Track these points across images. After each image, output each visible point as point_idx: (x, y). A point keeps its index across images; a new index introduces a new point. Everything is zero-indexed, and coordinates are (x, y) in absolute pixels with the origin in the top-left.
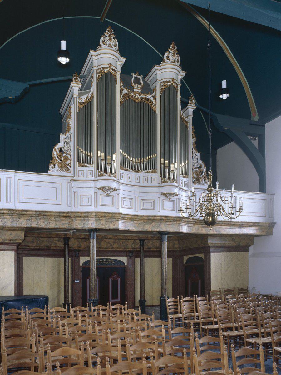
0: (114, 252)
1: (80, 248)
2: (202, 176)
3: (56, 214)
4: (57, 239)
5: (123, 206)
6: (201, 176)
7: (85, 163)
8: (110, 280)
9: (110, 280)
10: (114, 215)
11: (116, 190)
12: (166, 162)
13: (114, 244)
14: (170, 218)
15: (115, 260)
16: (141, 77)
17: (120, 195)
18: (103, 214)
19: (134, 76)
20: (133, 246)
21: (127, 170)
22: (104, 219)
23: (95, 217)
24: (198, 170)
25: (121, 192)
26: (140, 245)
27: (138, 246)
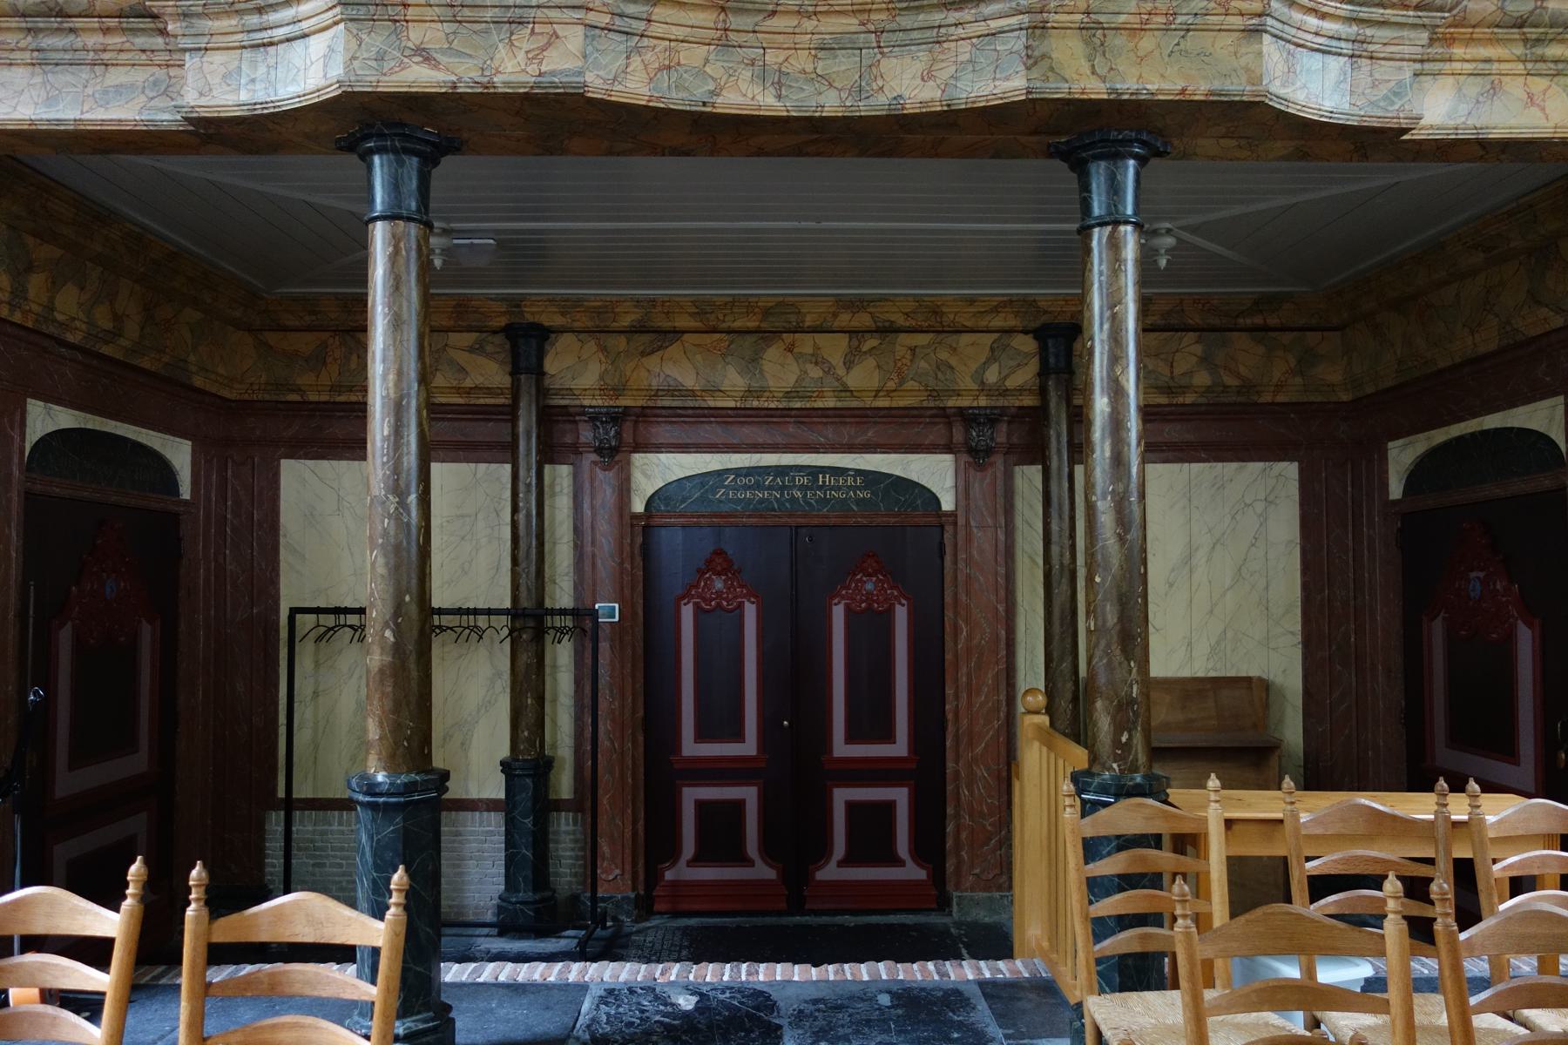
0: (863, 416)
1: (618, 391)
4: (469, 338)
8: (838, 613)
9: (838, 613)
13: (849, 365)
15: (872, 478)
20: (992, 376)
26: (1044, 373)
27: (1025, 375)
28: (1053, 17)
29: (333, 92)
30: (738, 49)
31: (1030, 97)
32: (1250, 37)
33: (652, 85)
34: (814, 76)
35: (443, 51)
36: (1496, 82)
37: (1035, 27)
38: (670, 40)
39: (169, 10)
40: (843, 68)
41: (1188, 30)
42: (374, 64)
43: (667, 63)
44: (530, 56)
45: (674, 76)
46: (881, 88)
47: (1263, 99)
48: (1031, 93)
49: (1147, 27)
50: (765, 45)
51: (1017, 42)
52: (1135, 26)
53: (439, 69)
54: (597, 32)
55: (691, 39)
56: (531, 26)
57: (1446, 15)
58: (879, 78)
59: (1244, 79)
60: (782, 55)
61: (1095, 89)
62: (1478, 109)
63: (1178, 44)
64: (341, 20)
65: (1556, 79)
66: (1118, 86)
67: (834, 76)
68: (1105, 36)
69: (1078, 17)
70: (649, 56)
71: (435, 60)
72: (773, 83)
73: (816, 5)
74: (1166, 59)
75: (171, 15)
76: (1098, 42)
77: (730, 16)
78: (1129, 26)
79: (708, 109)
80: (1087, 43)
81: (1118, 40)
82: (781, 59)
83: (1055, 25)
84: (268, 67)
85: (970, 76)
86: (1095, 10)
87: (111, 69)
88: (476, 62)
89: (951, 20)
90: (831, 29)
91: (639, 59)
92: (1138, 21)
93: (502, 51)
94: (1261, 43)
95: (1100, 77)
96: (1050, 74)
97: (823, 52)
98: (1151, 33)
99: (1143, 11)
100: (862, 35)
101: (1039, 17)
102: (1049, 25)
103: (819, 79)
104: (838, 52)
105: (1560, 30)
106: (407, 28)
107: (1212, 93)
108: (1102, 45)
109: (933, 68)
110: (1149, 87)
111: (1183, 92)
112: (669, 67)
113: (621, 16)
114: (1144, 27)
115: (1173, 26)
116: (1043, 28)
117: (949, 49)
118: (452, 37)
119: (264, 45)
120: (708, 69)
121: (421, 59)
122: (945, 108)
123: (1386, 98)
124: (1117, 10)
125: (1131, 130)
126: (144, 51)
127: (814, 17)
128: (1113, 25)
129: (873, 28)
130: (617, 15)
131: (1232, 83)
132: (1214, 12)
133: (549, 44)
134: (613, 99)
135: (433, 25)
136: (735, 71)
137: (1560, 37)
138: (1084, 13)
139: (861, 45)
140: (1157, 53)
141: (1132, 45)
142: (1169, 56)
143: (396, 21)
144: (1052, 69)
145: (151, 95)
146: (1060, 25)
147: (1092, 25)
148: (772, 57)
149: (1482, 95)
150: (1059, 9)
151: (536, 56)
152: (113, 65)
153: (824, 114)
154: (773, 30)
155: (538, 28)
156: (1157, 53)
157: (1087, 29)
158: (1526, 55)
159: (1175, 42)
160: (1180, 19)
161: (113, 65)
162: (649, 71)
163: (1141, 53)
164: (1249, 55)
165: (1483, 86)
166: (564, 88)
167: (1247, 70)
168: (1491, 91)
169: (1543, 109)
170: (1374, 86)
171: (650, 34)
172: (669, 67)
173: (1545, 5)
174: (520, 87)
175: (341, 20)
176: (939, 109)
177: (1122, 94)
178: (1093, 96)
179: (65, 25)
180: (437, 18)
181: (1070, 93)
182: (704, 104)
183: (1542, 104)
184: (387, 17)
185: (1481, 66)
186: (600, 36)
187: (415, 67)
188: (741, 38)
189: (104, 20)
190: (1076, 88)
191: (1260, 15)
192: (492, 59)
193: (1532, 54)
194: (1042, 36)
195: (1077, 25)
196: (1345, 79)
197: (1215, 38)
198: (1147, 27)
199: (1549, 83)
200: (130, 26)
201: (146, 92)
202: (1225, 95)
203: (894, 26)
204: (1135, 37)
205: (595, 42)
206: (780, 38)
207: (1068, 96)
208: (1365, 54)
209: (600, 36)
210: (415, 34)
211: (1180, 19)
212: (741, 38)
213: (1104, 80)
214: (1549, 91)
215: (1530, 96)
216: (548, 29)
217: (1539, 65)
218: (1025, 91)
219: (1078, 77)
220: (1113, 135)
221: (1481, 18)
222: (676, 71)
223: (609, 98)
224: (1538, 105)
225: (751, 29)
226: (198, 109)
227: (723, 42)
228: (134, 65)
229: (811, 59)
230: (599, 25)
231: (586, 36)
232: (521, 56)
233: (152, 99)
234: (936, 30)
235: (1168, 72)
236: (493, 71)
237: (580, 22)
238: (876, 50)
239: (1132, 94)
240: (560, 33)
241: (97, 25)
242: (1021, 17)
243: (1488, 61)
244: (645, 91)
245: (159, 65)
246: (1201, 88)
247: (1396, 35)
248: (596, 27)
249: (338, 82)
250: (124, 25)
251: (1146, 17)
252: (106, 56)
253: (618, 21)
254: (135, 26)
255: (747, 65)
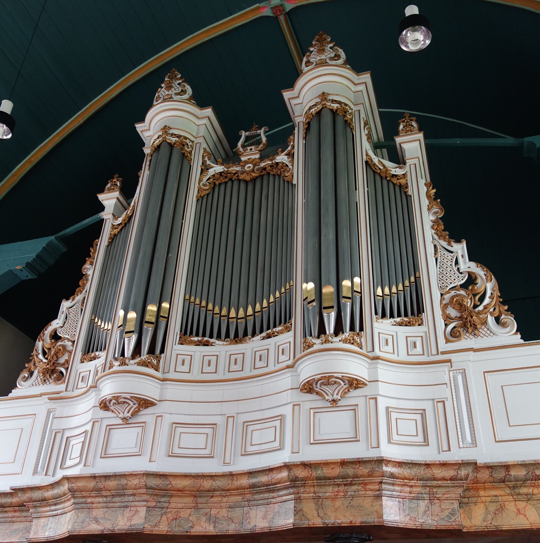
2: (485, 307)
3: (314, 474)
5: (395, 437)
6: (481, 308)
7: (211, 337)
10: (124, 481)
11: (152, 404)
12: (324, 290)
14: (326, 472)
16: (244, 134)
17: (379, 399)
18: (92, 484)
19: (262, 132)
21: (207, 344)
22: (101, 500)
23: (74, 497)
24: (462, 292)
25: (382, 388)
28: (302, 495)
29: (67, 535)
30: (202, 510)
31: (295, 527)
32: (377, 498)
33: (169, 526)
34: (227, 518)
35: (102, 518)
36: (502, 504)
37: (297, 499)
38: (178, 509)
39: (30, 505)
40: (237, 515)
41: (354, 497)
42: (80, 524)
43: (176, 517)
44: (128, 519)
45: (178, 521)
46: (249, 522)
47: (383, 524)
48: (294, 525)
49: (337, 497)
50: (210, 508)
51: (291, 504)
52: (333, 497)
53: (100, 525)
54: (151, 508)
55: (185, 508)
56: (130, 508)
57: (464, 482)
58: (249, 519)
59: (376, 516)
60: (217, 511)
61: (318, 522)
62: (496, 517)
63: (350, 503)
64: (74, 509)
65: (529, 502)
66: (326, 521)
67: (234, 518)
68: (322, 501)
69: (311, 495)
70: (169, 515)
71: (99, 522)
72: (213, 522)
73: (226, 493)
74: (346, 509)
75: (31, 507)
76: (320, 504)
77: (198, 498)
78: (330, 497)
79: (188, 534)
80: (316, 504)
81: (328, 503)
82: (216, 512)
83: (303, 498)
84: (55, 523)
85: (277, 518)
86: (318, 492)
87: (15, 523)
88: (111, 522)
89: (271, 497)
90: (232, 501)
91: (166, 517)
92: (334, 495)
93: (120, 517)
94: (382, 501)
95: (321, 517)
96: (303, 517)
97: (231, 509)
98: (340, 499)
99: (335, 491)
100: (244, 502)
101: (297, 495)
102: (301, 498)
103: (229, 519)
104: (236, 509)
105: (522, 482)
106: (93, 511)
107: (362, 522)
108: (322, 504)
109: (267, 514)
110: (338, 521)
111: (351, 522)
112: (176, 518)
113: (160, 502)
114: (336, 497)
115: (347, 496)
116: (300, 499)
117: (272, 507)
118: (105, 513)
119: (55, 515)
120: (190, 518)
121: (95, 522)
122: (269, 531)
123: (448, 516)
124: (325, 491)
125: (348, 533)
126: (25, 517)
127: (226, 497)
128: (324, 497)
129: (246, 500)
130: (158, 502)
131: (371, 518)
132: (361, 490)
133: (135, 514)
134: (154, 533)
135: (101, 509)
136: (200, 518)
137: (523, 485)
138: (313, 493)
139: (243, 506)
140: (342, 507)
141: (332, 504)
142: (347, 508)
143: (89, 509)
144: (303, 515)
145: (24, 532)
146: (305, 498)
147: (317, 497)
148: (214, 512)
149: (497, 510)
150: (304, 492)
151: (130, 519)
152: (15, 522)
153: (229, 534)
154: (212, 502)
155: (132, 509)
156: (342, 507)
157: (316, 499)
158: (511, 493)
159: (349, 502)
160: (349, 494)
161: (15, 522)
162: (169, 520)
163: (336, 507)
164: (377, 506)
165: (497, 507)
166: (137, 530)
167: (377, 512)
168: (501, 509)
169: (525, 516)
170: (442, 511)
171: (169, 507)
172: (176, 518)
173: (509, 474)
174: (123, 531)
175: (74, 509)
176: (267, 531)
177: (328, 524)
178: (318, 526)
179: (4, 510)
180: (101, 507)
181: (309, 525)
182: (187, 532)
183: (524, 513)
184: (87, 508)
185: (494, 498)
186: (152, 510)
187: (93, 525)
188: (202, 506)
189: (14, 508)
190: (310, 523)
191: (379, 490)
192: (116, 521)
193: (514, 492)
194: (300, 502)
195: (312, 498)
196: (428, 509)
197: (364, 499)
198: (337, 497)
199: (526, 504)
200: (21, 509)
201: (23, 531)
202: (368, 523)
203: (253, 499)
204: (334, 501)
205: (150, 513)
206: (215, 505)
207: (308, 526)
208: (435, 498)
209: (152, 510)
210: (95, 513)
211: (349, 494)
212: (202, 506)
213: (322, 518)
214: (527, 507)
215: (519, 510)
216: (135, 509)
217: (519, 497)
218: (292, 525)
219: (313, 518)
220: (341, 535)
221: (485, 480)
222: (179, 520)
223: (152, 533)
224: (523, 514)
225: (205, 502)
226: (32, 539)
227: (196, 508)
228: (21, 522)
229: (227, 511)
230: (151, 506)
231: (147, 511)
232: (125, 519)
233: (24, 533)
234: (267, 500)
235: (347, 514)
236: (116, 525)
237: (145, 506)
238: (249, 507)
239: (332, 524)
240: (139, 510)
241: (12, 510)
242: (292, 496)
243: (496, 496)
244: (166, 529)
245: (29, 521)
246: (358, 521)
247: (447, 490)
248: (150, 507)
249: (68, 531)
250: (20, 509)
251: (336, 493)
252: (14, 519)
253: (158, 504)
254: (23, 509)
255: (204, 515)
